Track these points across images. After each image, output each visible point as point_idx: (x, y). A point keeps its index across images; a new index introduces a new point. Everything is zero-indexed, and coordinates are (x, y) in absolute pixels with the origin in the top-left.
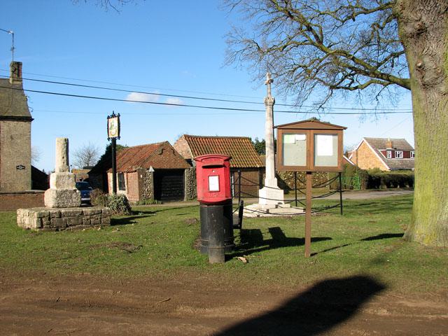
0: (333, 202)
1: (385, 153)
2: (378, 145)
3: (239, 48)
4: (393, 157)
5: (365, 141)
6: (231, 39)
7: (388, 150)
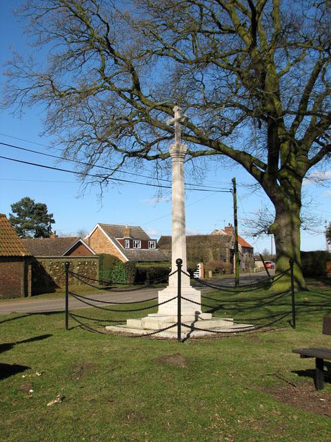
0: (307, 331)
1: (123, 242)
2: (114, 232)
3: (23, 84)
4: (131, 247)
5: (100, 227)
6: (14, 70)
7: (127, 239)
